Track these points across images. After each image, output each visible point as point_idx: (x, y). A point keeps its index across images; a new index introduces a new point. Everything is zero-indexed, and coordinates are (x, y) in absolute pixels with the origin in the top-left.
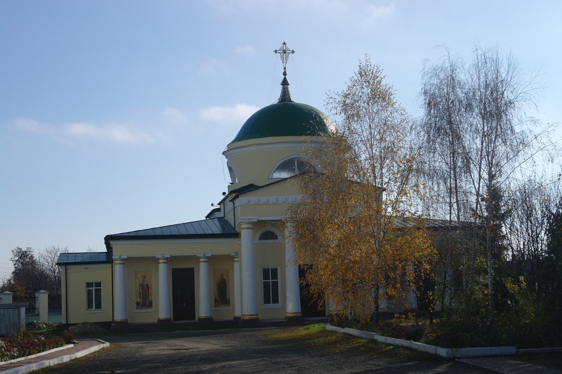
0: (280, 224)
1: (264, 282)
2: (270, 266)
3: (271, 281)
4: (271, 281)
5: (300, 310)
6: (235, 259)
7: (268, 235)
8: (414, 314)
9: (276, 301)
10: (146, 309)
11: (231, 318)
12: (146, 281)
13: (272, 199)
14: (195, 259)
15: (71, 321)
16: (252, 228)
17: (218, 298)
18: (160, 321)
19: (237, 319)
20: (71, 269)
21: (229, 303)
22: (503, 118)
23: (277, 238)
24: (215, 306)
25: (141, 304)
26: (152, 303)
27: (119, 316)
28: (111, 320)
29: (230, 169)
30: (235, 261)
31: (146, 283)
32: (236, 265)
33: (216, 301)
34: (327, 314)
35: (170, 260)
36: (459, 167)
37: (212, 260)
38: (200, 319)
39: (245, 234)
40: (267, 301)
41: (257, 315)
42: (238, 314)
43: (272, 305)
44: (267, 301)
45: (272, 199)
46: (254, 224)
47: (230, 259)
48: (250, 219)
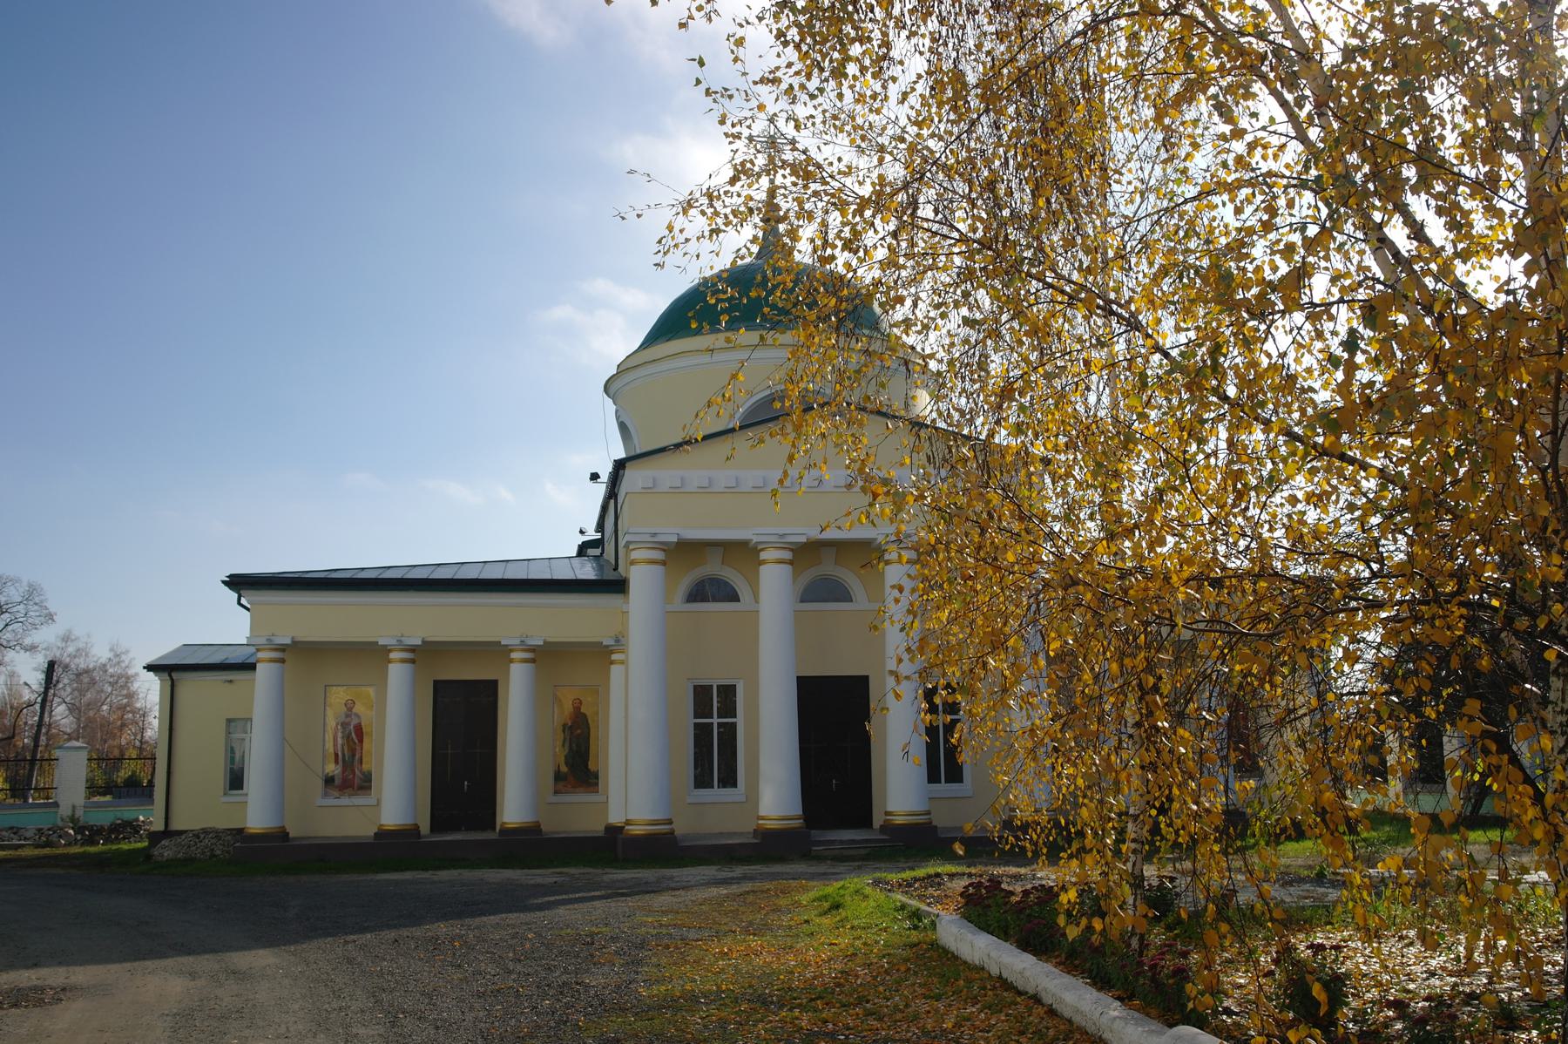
0: (743, 552)
1: (696, 725)
2: (716, 679)
3: (715, 720)
4: (715, 720)
5: (796, 808)
6: (614, 657)
7: (708, 591)
8: (1491, 786)
9: (729, 780)
10: (350, 795)
11: (597, 828)
12: (357, 715)
13: (724, 477)
14: (497, 652)
15: (177, 825)
16: (663, 563)
17: (564, 769)
18: (383, 835)
19: (614, 831)
20: (190, 686)
21: (597, 784)
22: (1358, 318)
23: (735, 598)
24: (556, 792)
25: (337, 782)
26: (370, 781)
27: (257, 814)
28: (161, 828)
29: (623, 427)
30: (612, 662)
31: (355, 721)
32: (616, 670)
33: (558, 777)
34: (878, 820)
35: (423, 654)
36: (1480, 117)
37: (546, 656)
38: (506, 832)
39: (643, 579)
40: (702, 781)
41: (670, 822)
42: (615, 818)
43: (716, 794)
44: (702, 781)
45: (724, 477)
46: (664, 547)
47: (600, 655)
48: (654, 535)
